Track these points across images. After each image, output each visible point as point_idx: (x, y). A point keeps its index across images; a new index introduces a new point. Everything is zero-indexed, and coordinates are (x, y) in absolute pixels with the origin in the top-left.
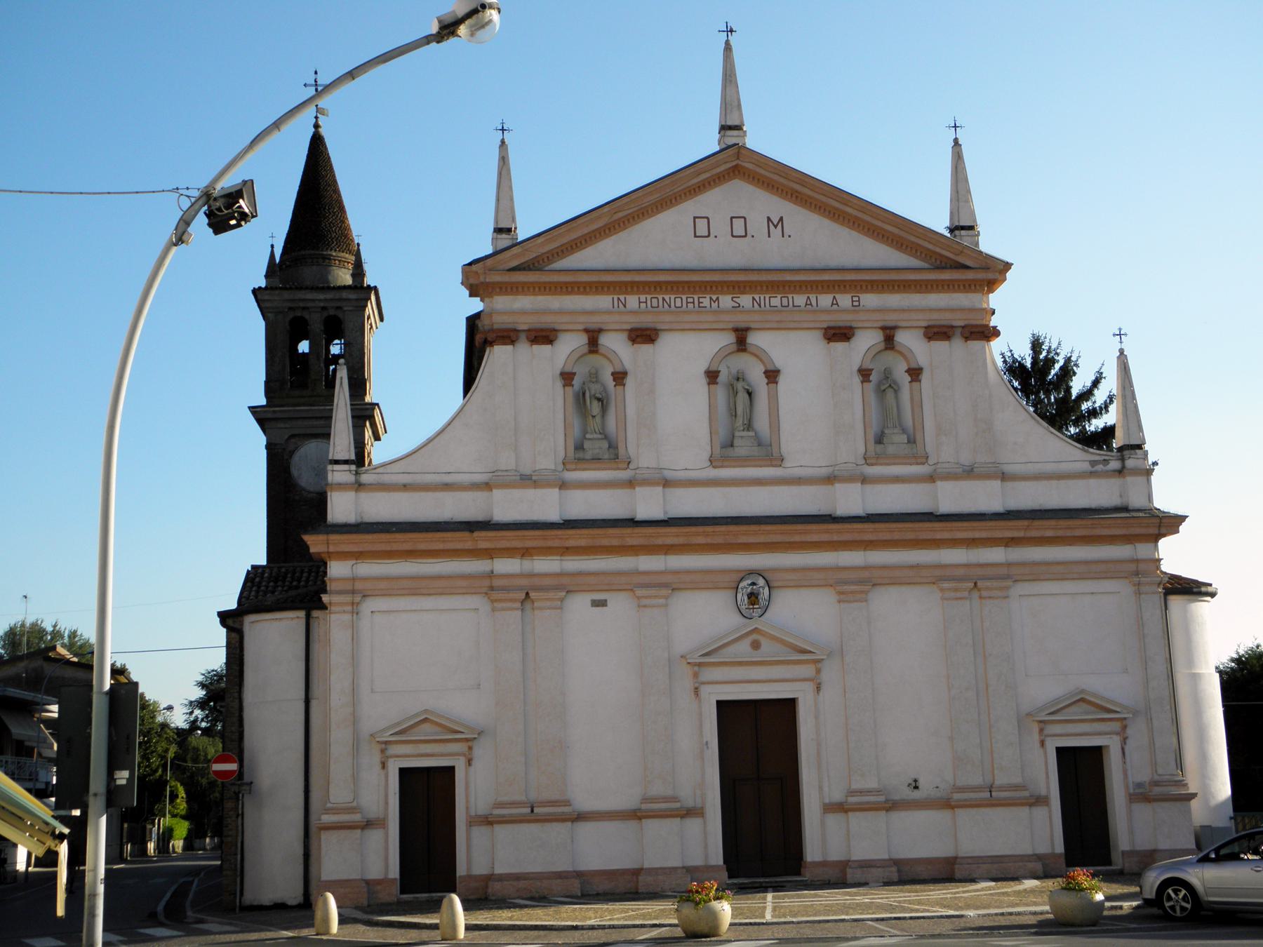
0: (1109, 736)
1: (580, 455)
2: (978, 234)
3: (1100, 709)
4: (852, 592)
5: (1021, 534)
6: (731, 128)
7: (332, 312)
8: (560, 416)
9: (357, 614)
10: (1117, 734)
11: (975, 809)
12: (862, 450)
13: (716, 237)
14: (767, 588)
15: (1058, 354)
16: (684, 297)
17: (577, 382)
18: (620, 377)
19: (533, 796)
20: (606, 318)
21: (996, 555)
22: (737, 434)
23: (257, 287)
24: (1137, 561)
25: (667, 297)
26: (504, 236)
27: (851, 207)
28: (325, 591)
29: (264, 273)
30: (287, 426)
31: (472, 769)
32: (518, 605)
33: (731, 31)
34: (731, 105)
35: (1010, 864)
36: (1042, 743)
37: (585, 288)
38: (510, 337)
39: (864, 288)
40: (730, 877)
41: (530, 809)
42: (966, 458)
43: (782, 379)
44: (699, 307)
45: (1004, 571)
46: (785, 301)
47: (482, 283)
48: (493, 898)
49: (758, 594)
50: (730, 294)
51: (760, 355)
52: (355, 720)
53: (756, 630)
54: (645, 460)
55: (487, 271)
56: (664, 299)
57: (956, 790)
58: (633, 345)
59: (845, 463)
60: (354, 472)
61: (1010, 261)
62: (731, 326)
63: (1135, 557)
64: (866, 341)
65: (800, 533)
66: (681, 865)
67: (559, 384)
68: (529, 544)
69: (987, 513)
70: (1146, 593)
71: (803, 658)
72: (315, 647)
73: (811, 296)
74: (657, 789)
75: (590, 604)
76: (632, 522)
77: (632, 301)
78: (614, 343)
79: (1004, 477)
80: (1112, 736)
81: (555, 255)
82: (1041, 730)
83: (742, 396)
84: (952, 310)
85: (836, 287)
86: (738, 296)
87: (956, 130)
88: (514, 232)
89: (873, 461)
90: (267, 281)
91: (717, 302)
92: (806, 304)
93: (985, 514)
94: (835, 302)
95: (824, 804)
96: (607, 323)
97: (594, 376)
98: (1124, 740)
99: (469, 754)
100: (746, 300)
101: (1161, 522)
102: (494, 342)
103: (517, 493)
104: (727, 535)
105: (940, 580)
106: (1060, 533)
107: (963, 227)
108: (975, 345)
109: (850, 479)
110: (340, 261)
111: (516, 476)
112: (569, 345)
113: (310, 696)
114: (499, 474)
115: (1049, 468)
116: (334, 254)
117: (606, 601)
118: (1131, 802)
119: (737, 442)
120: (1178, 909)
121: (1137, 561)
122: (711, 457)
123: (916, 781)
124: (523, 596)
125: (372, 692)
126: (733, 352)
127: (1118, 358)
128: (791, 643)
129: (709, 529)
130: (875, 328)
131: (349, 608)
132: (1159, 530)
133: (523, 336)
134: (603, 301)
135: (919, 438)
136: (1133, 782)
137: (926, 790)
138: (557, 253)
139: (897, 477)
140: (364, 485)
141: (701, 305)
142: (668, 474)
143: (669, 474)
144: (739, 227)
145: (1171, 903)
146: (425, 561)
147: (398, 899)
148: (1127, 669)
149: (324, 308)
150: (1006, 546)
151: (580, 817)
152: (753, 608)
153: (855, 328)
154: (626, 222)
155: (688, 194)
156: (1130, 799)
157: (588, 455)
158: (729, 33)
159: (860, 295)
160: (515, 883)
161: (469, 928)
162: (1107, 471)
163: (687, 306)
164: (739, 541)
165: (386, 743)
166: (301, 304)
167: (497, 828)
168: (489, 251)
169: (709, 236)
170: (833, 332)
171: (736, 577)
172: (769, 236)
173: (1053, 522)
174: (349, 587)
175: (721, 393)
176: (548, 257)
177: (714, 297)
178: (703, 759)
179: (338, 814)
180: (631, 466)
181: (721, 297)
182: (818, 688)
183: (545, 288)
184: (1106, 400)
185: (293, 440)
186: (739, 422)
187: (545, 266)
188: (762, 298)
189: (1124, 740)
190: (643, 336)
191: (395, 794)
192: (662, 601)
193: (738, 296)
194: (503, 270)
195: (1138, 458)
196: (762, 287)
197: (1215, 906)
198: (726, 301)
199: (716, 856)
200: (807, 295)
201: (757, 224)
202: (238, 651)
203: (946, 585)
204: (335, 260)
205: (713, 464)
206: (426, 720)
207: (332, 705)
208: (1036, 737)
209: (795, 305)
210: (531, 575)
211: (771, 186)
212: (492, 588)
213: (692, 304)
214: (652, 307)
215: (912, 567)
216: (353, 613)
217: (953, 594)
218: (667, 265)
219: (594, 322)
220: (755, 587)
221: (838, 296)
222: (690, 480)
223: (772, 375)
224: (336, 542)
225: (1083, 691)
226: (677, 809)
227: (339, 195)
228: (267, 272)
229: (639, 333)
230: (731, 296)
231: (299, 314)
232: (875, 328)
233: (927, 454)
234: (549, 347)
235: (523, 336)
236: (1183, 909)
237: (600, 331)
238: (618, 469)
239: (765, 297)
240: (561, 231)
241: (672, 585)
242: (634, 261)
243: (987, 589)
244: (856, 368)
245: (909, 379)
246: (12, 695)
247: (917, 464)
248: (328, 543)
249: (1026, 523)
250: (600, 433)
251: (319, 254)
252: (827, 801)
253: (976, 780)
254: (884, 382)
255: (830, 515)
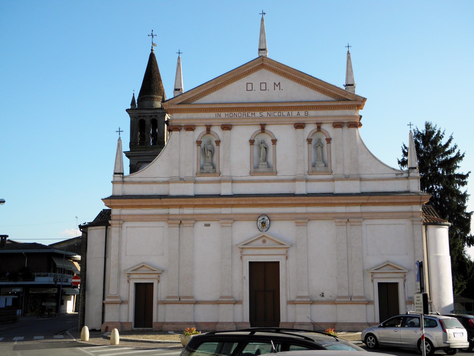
0: (398, 279)
1: (202, 171)
2: (355, 87)
3: (396, 269)
4: (301, 222)
5: (366, 201)
6: (262, 50)
7: (154, 117)
8: (196, 157)
9: (121, 228)
10: (402, 278)
11: (345, 305)
12: (307, 169)
13: (255, 90)
14: (268, 221)
15: (435, 130)
16: (242, 113)
17: (202, 145)
18: (218, 142)
19: (181, 295)
20: (213, 121)
21: (357, 209)
22: (260, 163)
23: (127, 109)
24: (413, 212)
25: (236, 113)
26: (177, 92)
27: (305, 78)
28: (110, 220)
29: (130, 104)
30: (137, 158)
31: (159, 284)
32: (178, 225)
33: (264, 14)
34: (262, 41)
35: (357, 326)
36: (372, 281)
37: (205, 110)
38: (178, 128)
39: (310, 108)
40: (251, 327)
41: (179, 299)
42: (347, 172)
43: (278, 143)
44: (247, 116)
45: (360, 215)
46: (280, 114)
47: (168, 109)
48: (164, 330)
49: (265, 223)
50: (259, 111)
51: (270, 134)
52: (119, 265)
53: (264, 236)
54: (225, 173)
55: (170, 105)
56: (234, 114)
57: (338, 298)
58: (223, 130)
59: (300, 174)
60: (122, 177)
61: (365, 97)
62: (259, 123)
63: (412, 211)
64: (310, 128)
65: (280, 200)
66: (232, 321)
67: (196, 145)
68: (181, 203)
69: (353, 193)
70: (416, 224)
71: (282, 247)
72: (109, 239)
73: (289, 112)
74: (226, 293)
75: (204, 225)
76: (219, 196)
77: (223, 115)
78: (216, 130)
79: (361, 180)
80: (400, 279)
81: (195, 98)
82: (372, 276)
83: (263, 150)
84: (344, 116)
85: (299, 108)
86: (262, 112)
87: (348, 48)
88: (181, 90)
89: (311, 173)
90: (131, 107)
91: (254, 115)
92: (288, 115)
93: (352, 194)
94: (298, 114)
95: (287, 301)
96: (213, 123)
97: (210, 142)
98: (405, 281)
99: (159, 278)
100: (265, 114)
101: (421, 197)
102: (172, 130)
103: (178, 185)
104: (254, 201)
105: (335, 218)
106: (381, 201)
107: (350, 85)
108: (352, 129)
109: (301, 180)
110: (157, 99)
111: (178, 179)
112: (200, 131)
113: (106, 257)
114: (172, 178)
115: (379, 176)
116: (155, 96)
117: (210, 224)
118: (406, 304)
119: (260, 166)
120: (371, 344)
121: (413, 212)
122: (250, 172)
123: (323, 293)
124: (179, 222)
125: (126, 256)
126: (260, 133)
127: (409, 134)
128: (279, 242)
129: (247, 198)
130: (314, 123)
131: (118, 226)
132: (421, 200)
133: (183, 128)
134: (212, 115)
135: (329, 164)
136: (408, 297)
137: (326, 297)
138: (196, 98)
139: (320, 179)
140: (125, 182)
141: (248, 116)
142: (234, 178)
143: (234, 178)
144: (264, 87)
145: (369, 342)
146: (144, 209)
147: (132, 329)
148: (407, 253)
149: (151, 116)
150: (361, 206)
151: (197, 303)
152: (263, 228)
153: (305, 124)
154: (221, 86)
155: (244, 75)
156: (406, 303)
157: (205, 171)
158: (263, 14)
159: (308, 111)
160: (172, 325)
161: (120, 340)
162: (402, 177)
163: (243, 116)
164: (258, 203)
165: (129, 274)
166: (143, 115)
167: (167, 305)
168: (173, 97)
169: (266, 90)
170: (297, 125)
171: (257, 216)
172: (275, 90)
173: (378, 197)
174: (119, 218)
175: (255, 148)
176: (193, 99)
177: (253, 113)
178: (243, 283)
179: (111, 298)
180: (221, 175)
181: (256, 113)
182: (287, 258)
183: (191, 110)
184: (454, 147)
185: (139, 164)
186: (261, 159)
187: (192, 102)
188: (271, 113)
189: (405, 281)
190: (227, 127)
191: (132, 292)
192: (230, 225)
193: (262, 112)
194: (176, 104)
195: (415, 173)
196: (271, 109)
197: (383, 344)
198: (258, 114)
199: (247, 318)
200: (288, 111)
201: (270, 86)
202: (85, 240)
203: (337, 220)
204: (156, 98)
205: (251, 174)
206: (143, 266)
207: (111, 260)
208: (370, 279)
209: (283, 115)
210: (183, 215)
211: (276, 71)
212: (169, 219)
213: (245, 116)
214: (230, 117)
215: (324, 213)
216: (119, 227)
217: (340, 224)
218: (236, 101)
219: (208, 122)
220: (264, 220)
221: (300, 112)
222: (242, 180)
223: (274, 141)
224: (113, 202)
225: (388, 261)
226: (232, 301)
227: (159, 75)
228: (131, 103)
229: (225, 126)
230: (259, 112)
231: (142, 118)
232: (314, 123)
233: (332, 171)
234: (192, 132)
235: (183, 128)
236: (373, 345)
237: (211, 126)
238: (216, 176)
239: (272, 113)
240: (197, 89)
241: (234, 219)
242: (224, 100)
243: (353, 222)
244: (306, 139)
245: (326, 142)
246: (55, 252)
247: (328, 174)
248: (111, 203)
249: (367, 197)
250: (210, 163)
251: (150, 97)
252: (289, 300)
253: (346, 294)
254: (317, 144)
255: (294, 194)
